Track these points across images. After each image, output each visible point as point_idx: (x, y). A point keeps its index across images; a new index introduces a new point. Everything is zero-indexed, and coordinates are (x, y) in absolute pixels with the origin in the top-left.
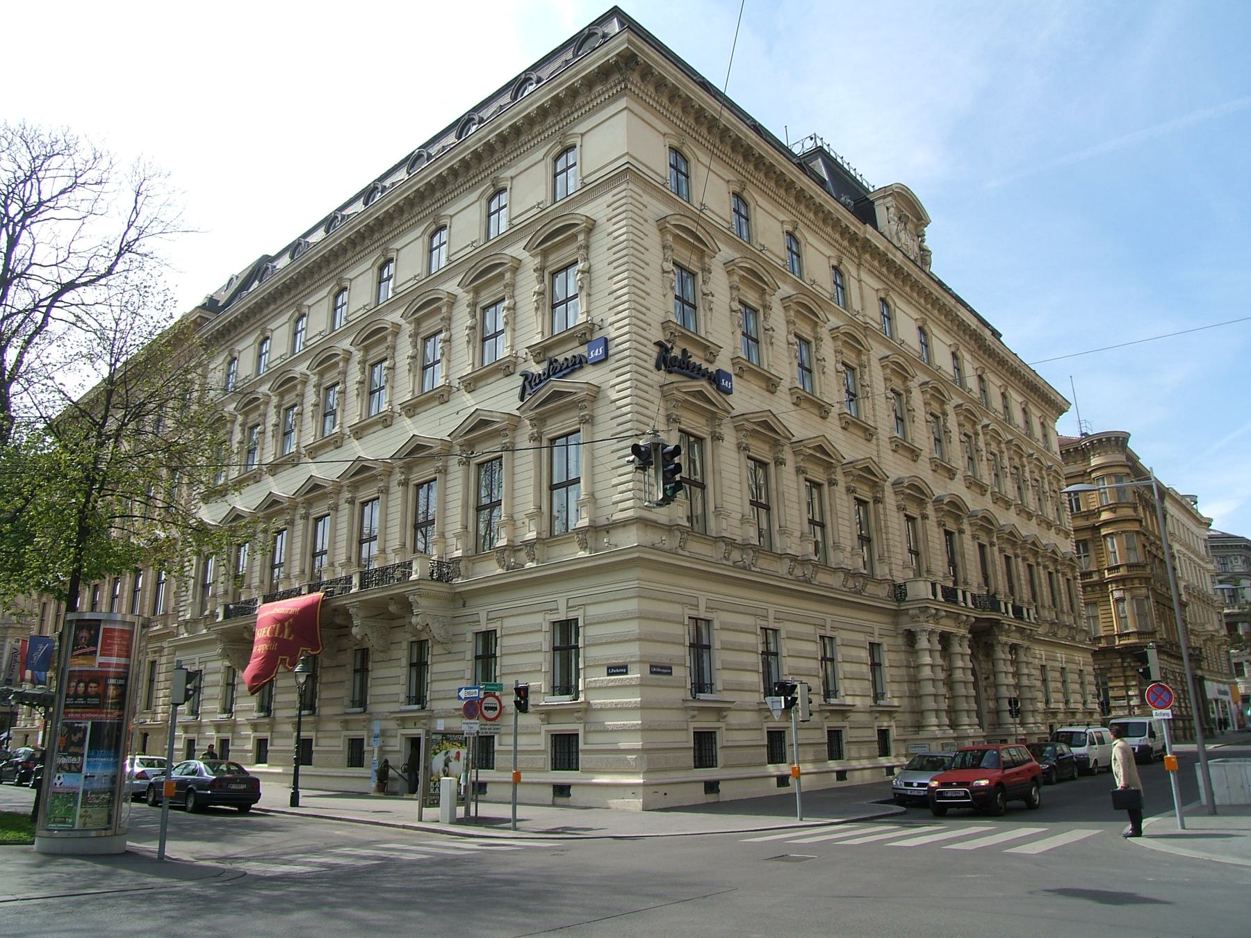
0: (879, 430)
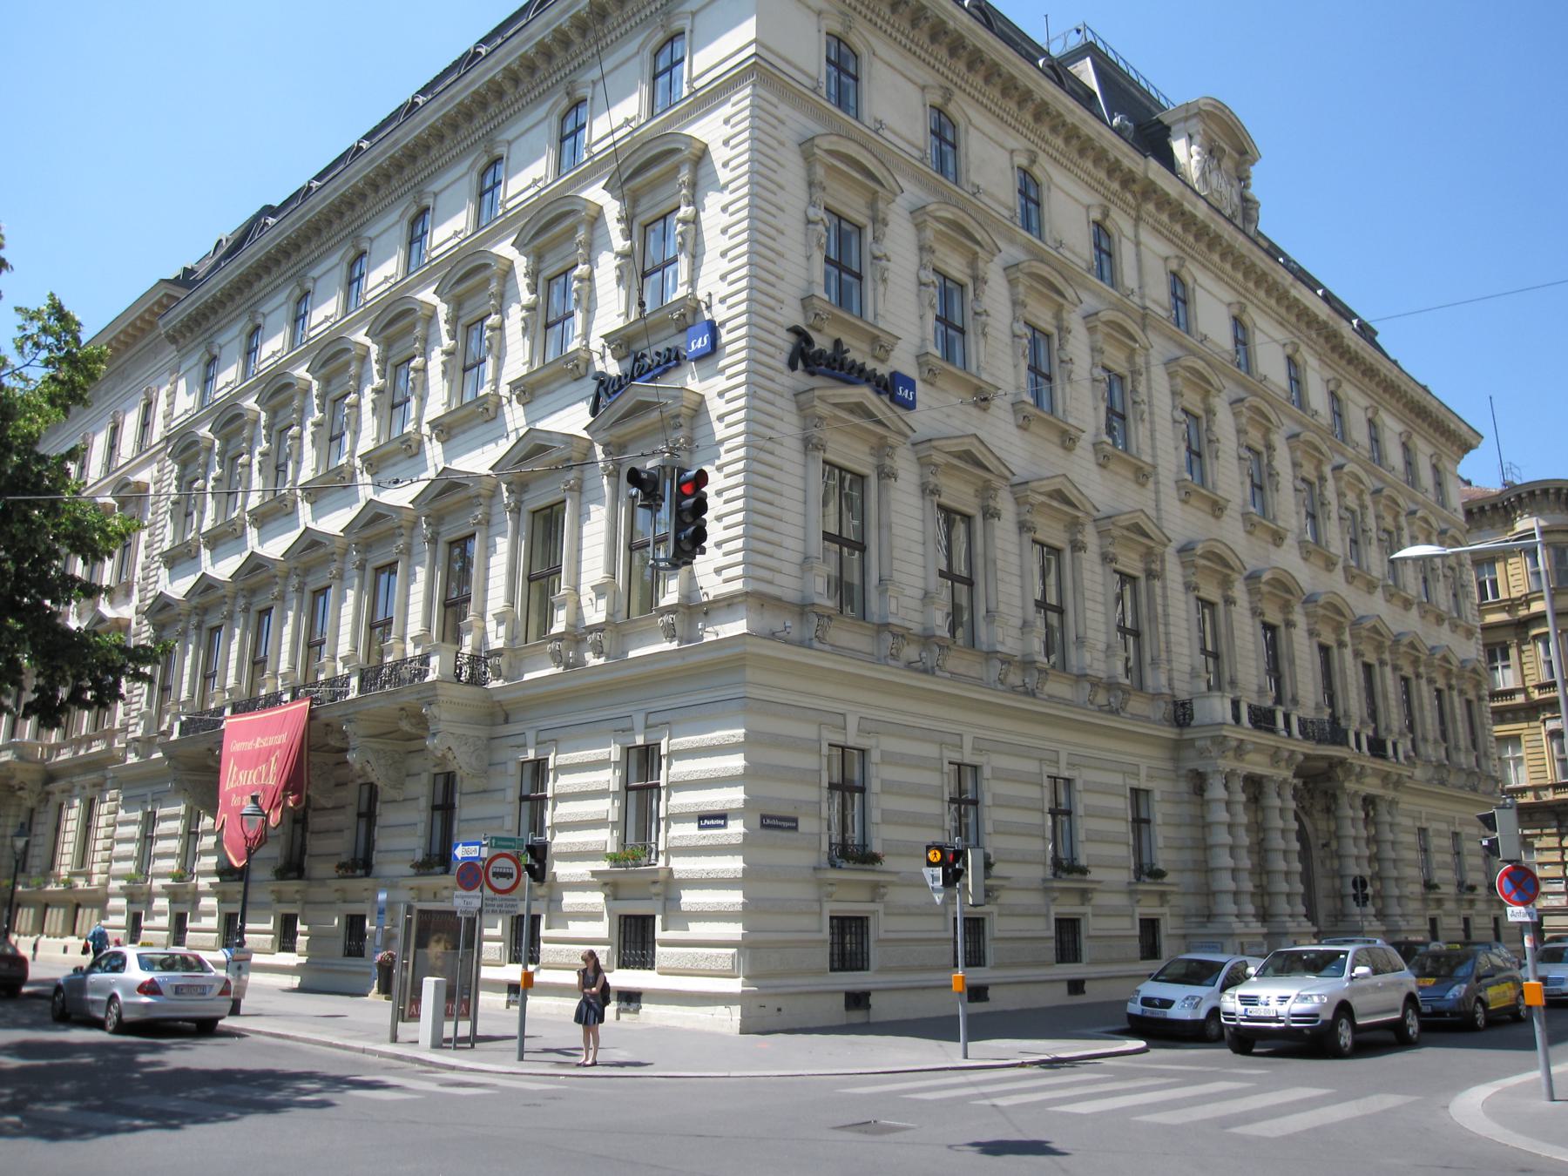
0: (1160, 469)
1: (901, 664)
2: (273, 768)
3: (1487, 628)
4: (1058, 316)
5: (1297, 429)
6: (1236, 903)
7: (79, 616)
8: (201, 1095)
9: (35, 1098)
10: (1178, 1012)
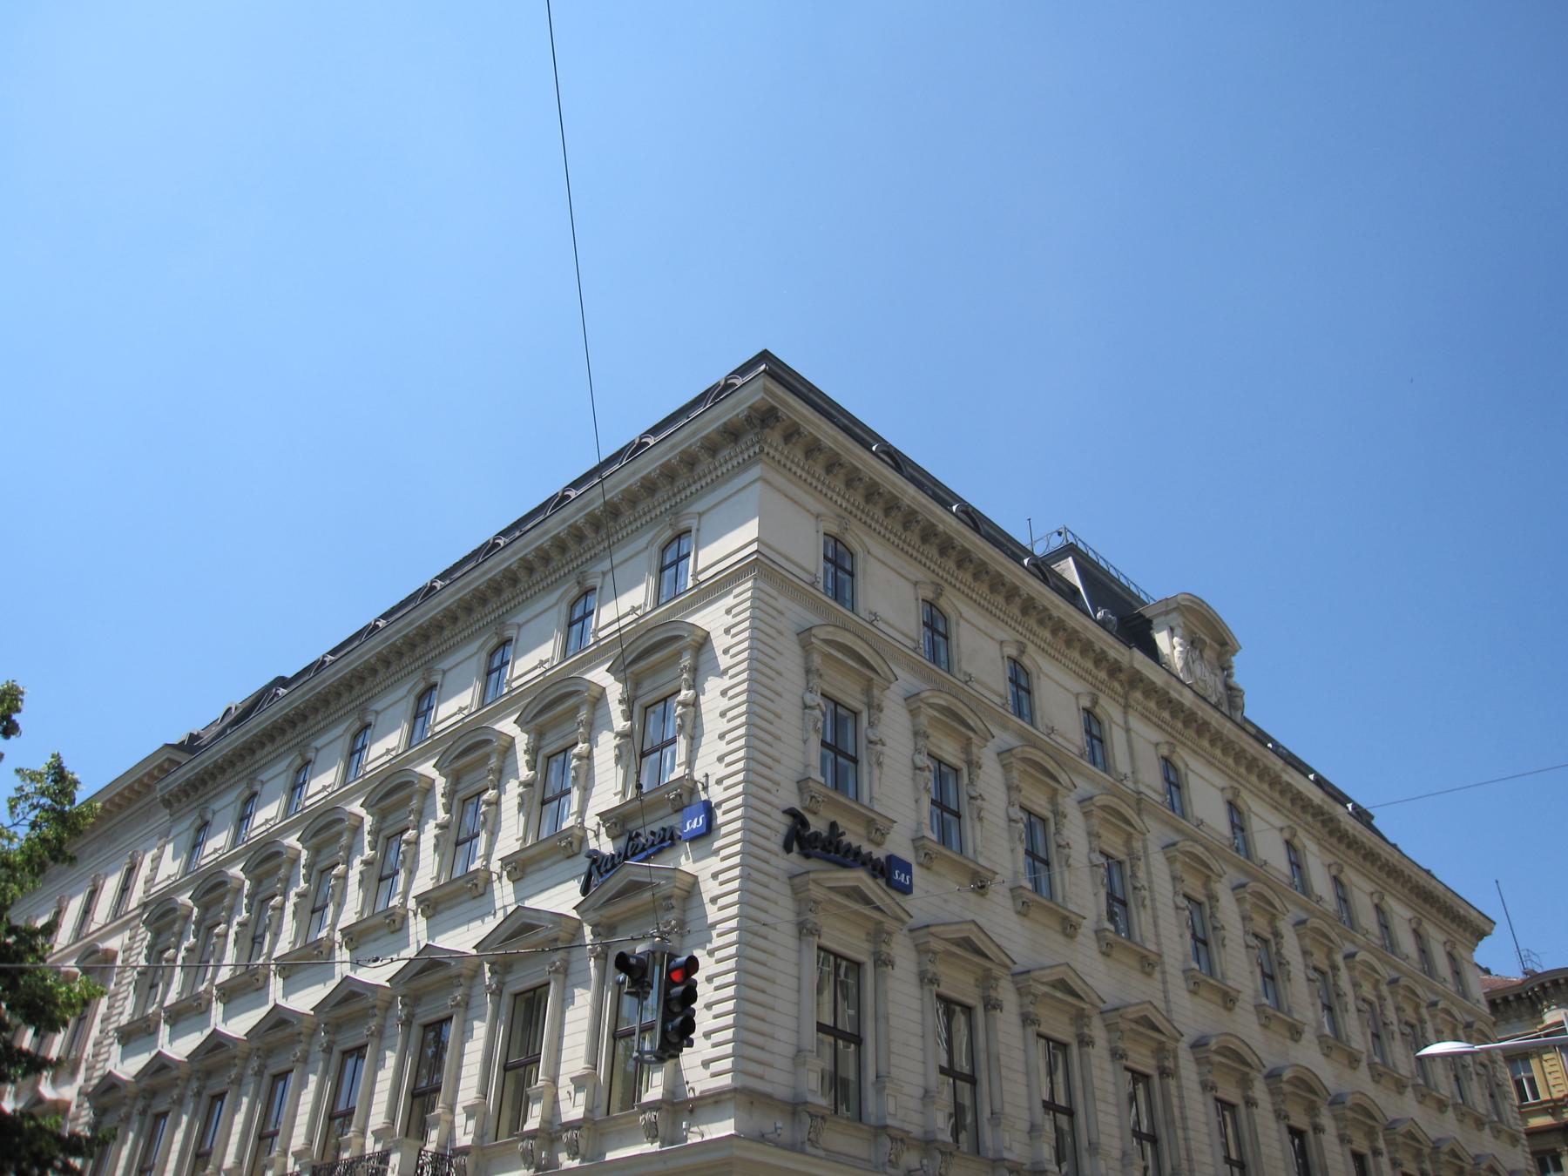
0: (1166, 958)
3: (1533, 1133)
4: (1053, 800)
5: (1304, 916)
7: (17, 1096)
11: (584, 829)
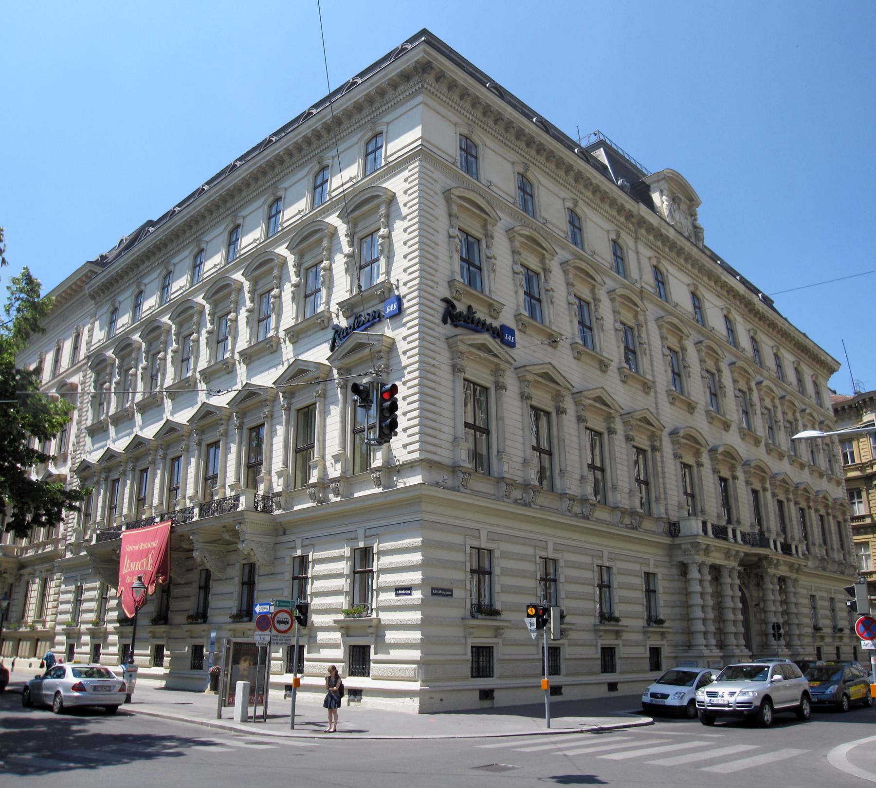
0: (657, 384)
1: (511, 501)
2: (150, 561)
3: (848, 480)
5: (734, 359)
6: (705, 638)
7: (37, 473)
8: (108, 749)
9: (12, 751)
10: (671, 701)
11: (330, 313)
